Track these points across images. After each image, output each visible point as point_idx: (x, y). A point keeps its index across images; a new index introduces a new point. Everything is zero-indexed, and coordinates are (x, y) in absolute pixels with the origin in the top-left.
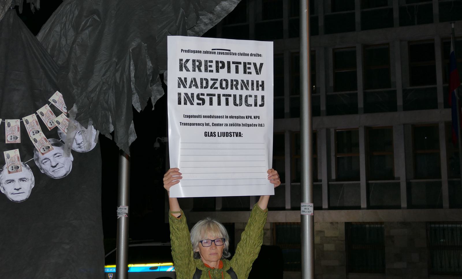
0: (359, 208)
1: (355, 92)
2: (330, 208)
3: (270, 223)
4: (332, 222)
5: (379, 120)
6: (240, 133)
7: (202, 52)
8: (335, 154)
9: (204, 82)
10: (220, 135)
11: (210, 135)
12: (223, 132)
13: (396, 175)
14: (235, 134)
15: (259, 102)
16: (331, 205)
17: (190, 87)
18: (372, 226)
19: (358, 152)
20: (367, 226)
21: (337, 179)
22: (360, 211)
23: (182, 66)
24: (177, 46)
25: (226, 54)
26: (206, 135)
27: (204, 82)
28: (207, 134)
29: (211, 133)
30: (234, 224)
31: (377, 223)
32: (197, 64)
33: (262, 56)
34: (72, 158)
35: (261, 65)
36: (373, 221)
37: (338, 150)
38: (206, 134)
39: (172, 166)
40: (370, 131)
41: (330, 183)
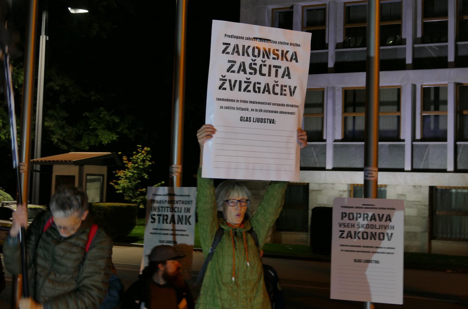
0: (444, 171)
2: (413, 170)
3: (348, 184)
7: (245, 38)
8: (421, 112)
10: (255, 121)
11: (245, 120)
14: (269, 120)
16: (415, 167)
17: (371, 220)
18: (459, 191)
19: (446, 111)
20: (454, 191)
24: (220, 29)
26: (241, 120)
28: (243, 119)
29: (247, 118)
30: (308, 184)
32: (366, 216)
35: (295, 87)
37: (425, 107)
38: (242, 119)
39: (207, 122)
41: (414, 143)
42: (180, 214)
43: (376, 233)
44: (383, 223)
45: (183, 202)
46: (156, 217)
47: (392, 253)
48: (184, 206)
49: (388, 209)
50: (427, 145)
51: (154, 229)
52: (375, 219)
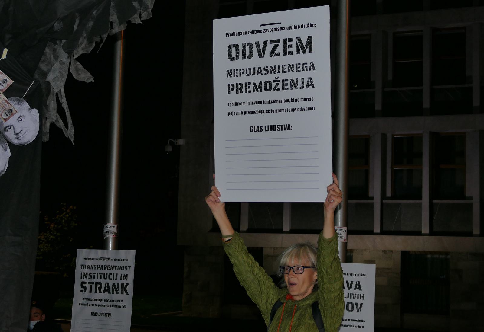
0: (419, 233)
1: (420, 88)
2: (384, 232)
4: (385, 249)
5: (448, 125)
6: (289, 125)
10: (267, 129)
11: (256, 130)
12: (270, 126)
13: (468, 194)
14: (283, 126)
15: (252, 73)
18: (435, 256)
19: (421, 164)
20: (429, 256)
21: (393, 197)
22: (421, 238)
25: (273, 30)
26: (252, 131)
28: (253, 129)
29: (258, 127)
31: (441, 253)
33: (315, 25)
34: (9, 153)
36: (436, 250)
37: (396, 161)
40: (437, 138)
41: (384, 201)
42: (116, 282)
44: (352, 291)
45: (119, 268)
46: (88, 286)
47: (362, 327)
48: (120, 272)
49: (358, 275)
50: (400, 204)
51: (84, 299)
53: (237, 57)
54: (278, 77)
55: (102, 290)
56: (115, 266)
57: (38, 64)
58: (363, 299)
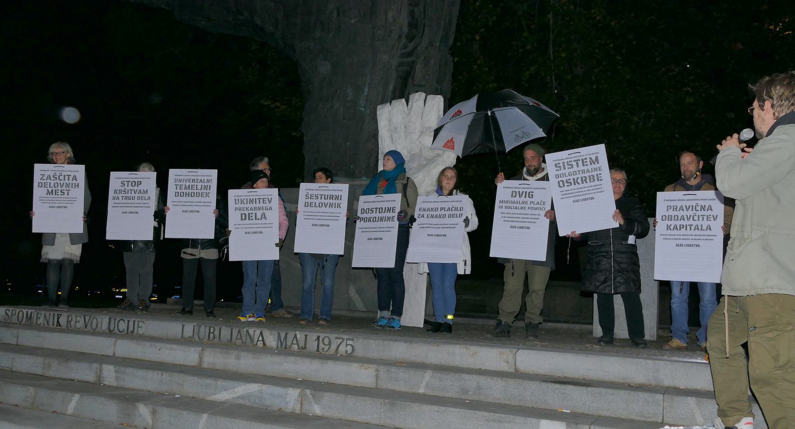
9: (676, 217)
23: (339, 206)
26: (677, 246)
27: (676, 217)
35: (717, 216)
38: (677, 245)
43: (253, 199)
52: (684, 219)
53: (666, 219)
54: (452, 138)
55: (678, 210)
56: (701, 216)
57: (41, 247)
58: (78, 188)
